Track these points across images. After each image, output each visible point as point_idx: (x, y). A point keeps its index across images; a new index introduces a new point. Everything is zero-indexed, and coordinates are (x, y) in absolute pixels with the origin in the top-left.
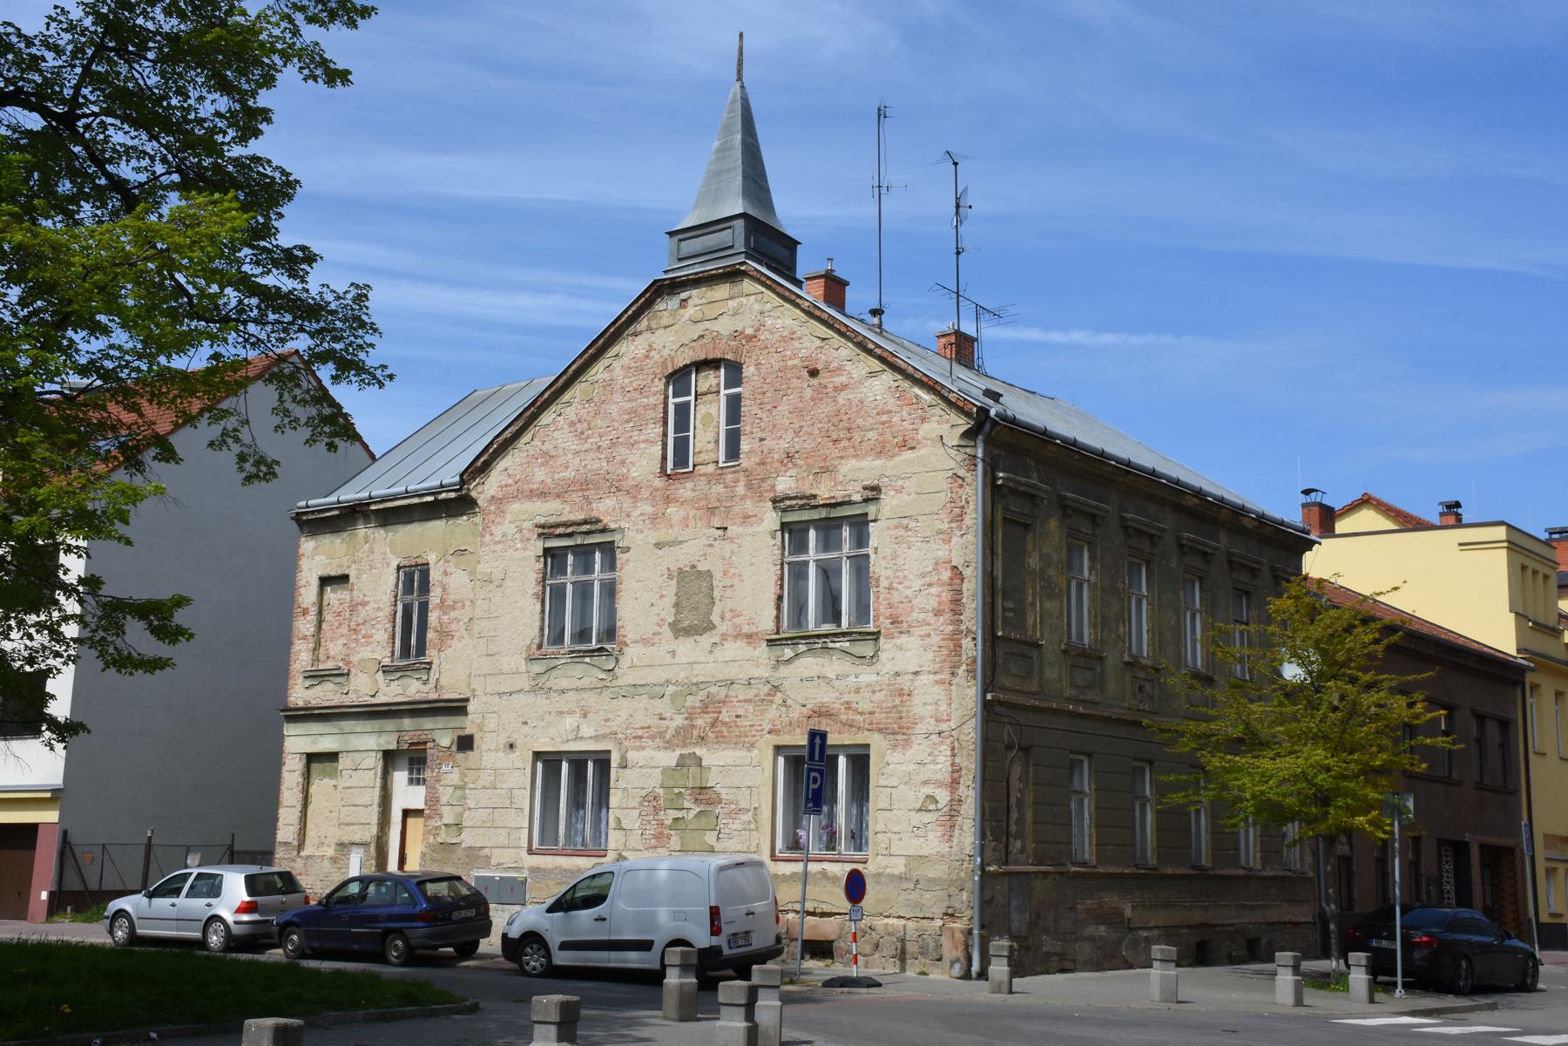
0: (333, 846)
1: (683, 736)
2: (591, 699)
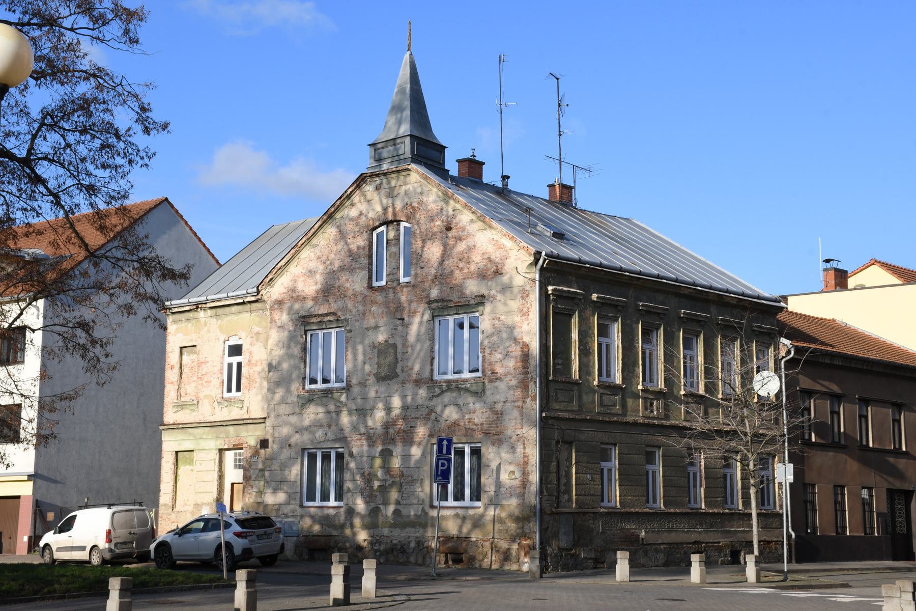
0: (192, 506)
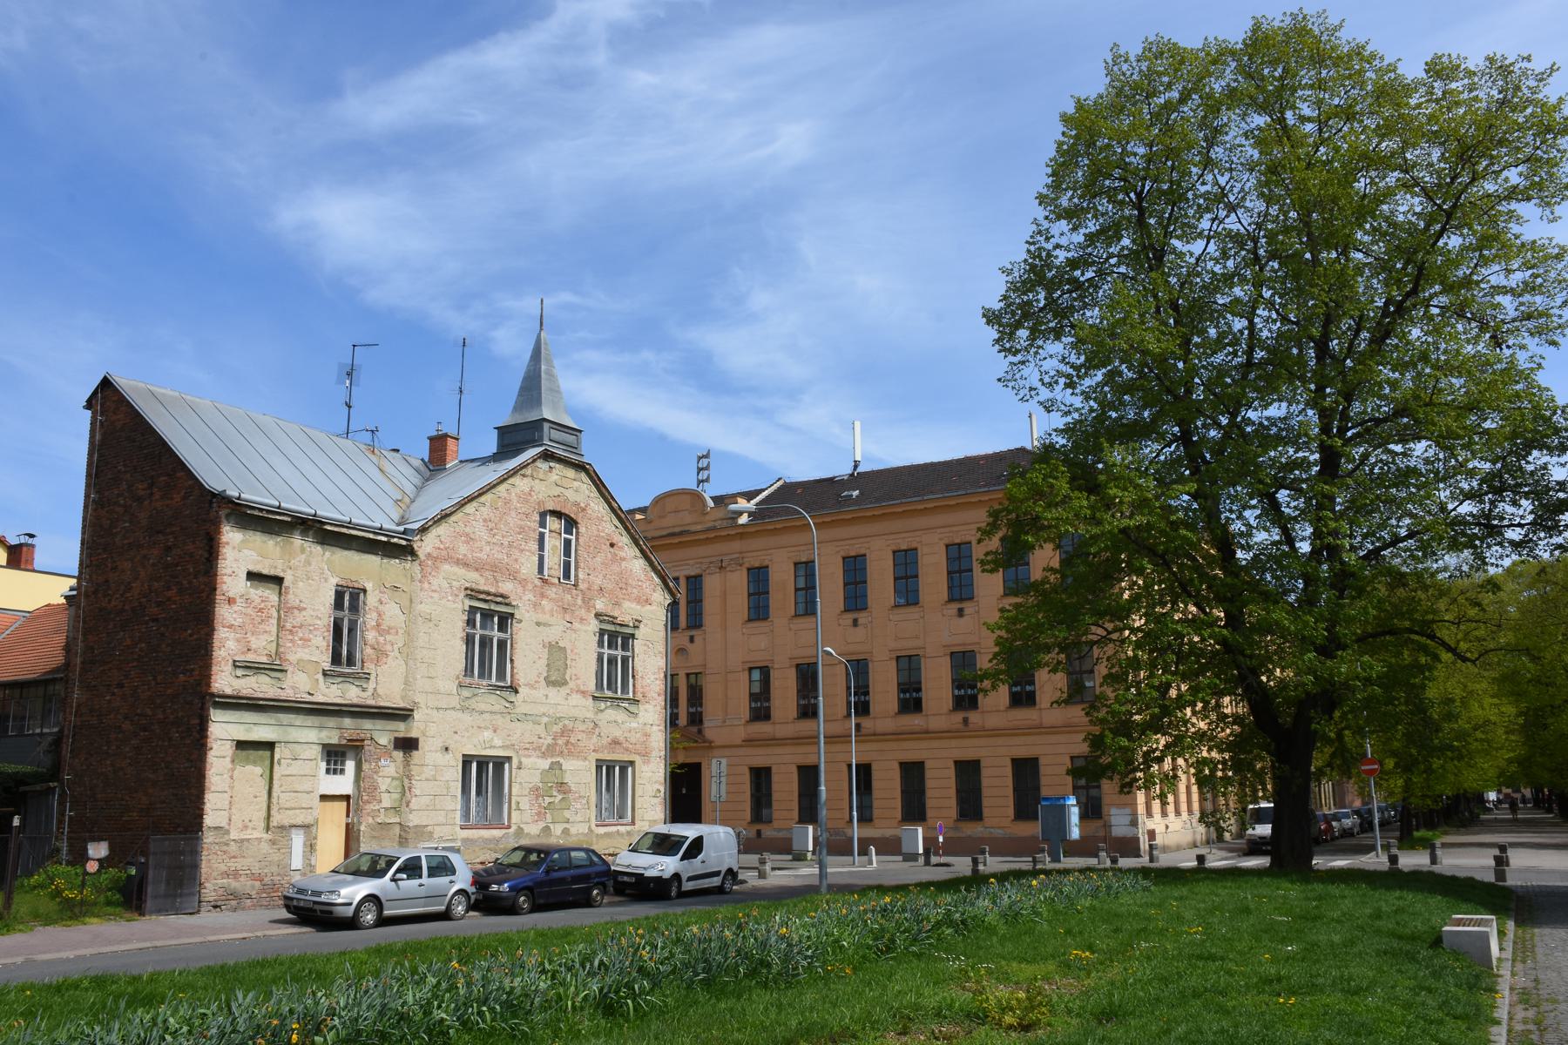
1: (549, 751)
2: (499, 720)
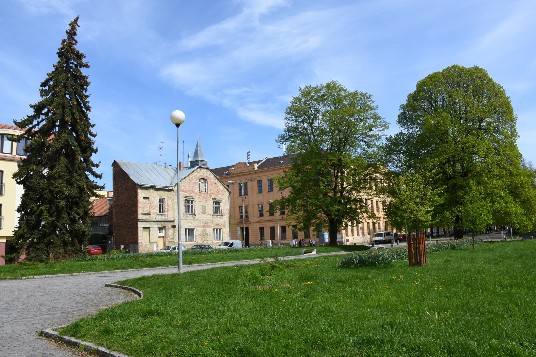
1: (203, 227)
2: (192, 221)
